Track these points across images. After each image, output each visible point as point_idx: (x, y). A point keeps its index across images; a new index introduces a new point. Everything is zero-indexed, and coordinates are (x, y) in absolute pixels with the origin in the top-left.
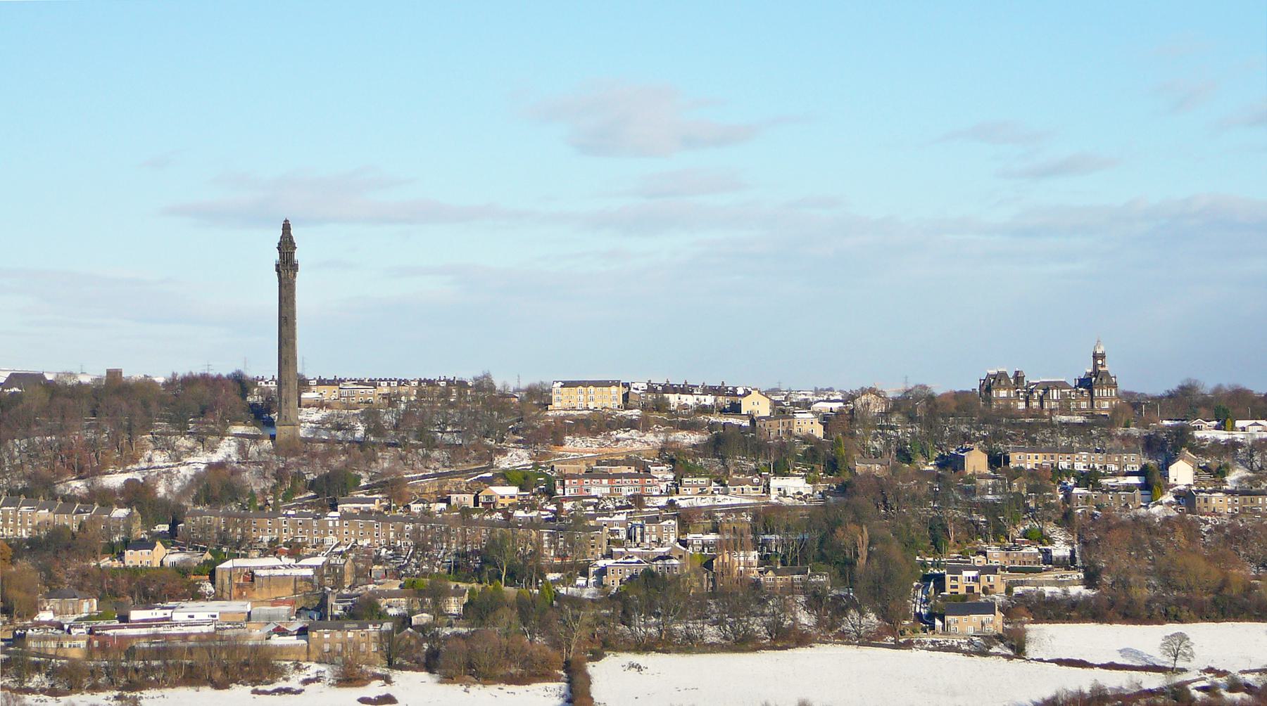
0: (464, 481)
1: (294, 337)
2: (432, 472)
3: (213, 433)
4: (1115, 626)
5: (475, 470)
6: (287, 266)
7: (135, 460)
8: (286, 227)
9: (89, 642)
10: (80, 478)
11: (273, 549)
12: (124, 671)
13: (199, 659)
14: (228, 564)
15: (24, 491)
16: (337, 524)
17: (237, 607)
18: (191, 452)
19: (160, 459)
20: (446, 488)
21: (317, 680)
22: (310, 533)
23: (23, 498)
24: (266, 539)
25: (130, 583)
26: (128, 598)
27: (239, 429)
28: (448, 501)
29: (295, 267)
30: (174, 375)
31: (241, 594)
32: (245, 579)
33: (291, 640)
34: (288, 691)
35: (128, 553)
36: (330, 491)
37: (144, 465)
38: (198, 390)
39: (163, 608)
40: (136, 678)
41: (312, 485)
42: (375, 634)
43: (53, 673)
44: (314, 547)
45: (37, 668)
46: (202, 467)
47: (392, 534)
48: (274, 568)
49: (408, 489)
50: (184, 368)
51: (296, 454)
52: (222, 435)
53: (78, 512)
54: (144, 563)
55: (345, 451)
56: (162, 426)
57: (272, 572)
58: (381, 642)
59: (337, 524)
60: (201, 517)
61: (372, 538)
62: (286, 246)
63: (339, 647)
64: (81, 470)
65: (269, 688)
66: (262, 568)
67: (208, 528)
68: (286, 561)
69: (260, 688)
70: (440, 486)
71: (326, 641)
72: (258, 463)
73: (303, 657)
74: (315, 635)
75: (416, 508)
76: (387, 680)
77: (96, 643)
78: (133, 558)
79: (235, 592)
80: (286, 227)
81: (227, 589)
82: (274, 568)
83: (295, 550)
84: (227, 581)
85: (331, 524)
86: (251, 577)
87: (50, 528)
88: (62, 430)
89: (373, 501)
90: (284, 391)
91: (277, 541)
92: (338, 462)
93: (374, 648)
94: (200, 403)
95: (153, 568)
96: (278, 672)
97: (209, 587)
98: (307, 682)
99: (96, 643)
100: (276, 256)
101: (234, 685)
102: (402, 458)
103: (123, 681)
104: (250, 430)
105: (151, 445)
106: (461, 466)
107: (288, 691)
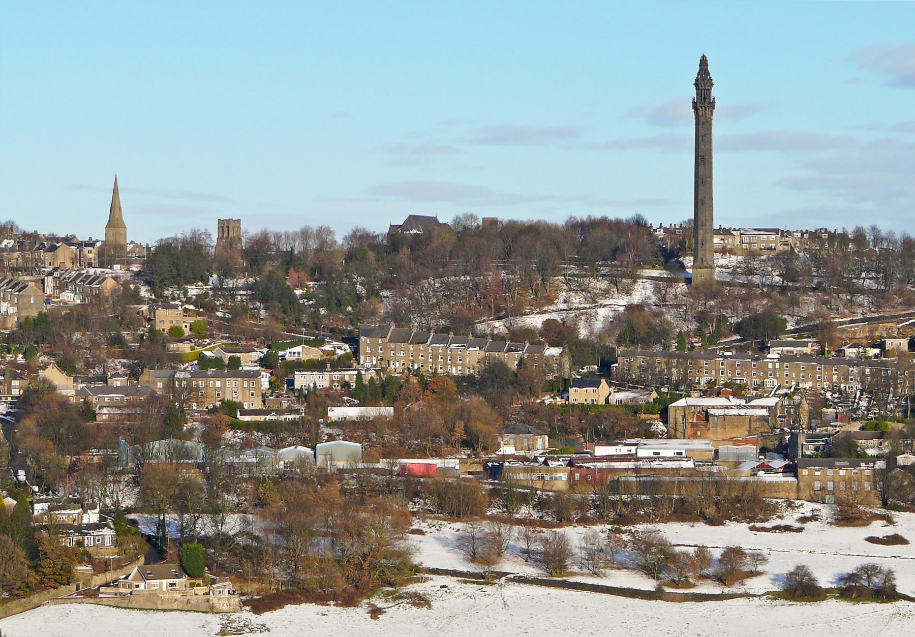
0: (895, 326)
1: (710, 176)
2: (859, 317)
3: (624, 276)
4: (303, 605)
5: (904, 315)
6: (703, 103)
7: (550, 302)
8: (704, 62)
9: (571, 474)
10: (499, 318)
11: (711, 390)
12: (614, 504)
13: (692, 495)
14: (681, 403)
15: (445, 330)
16: (777, 366)
17: (701, 445)
18: (606, 293)
19: (577, 300)
20: (877, 333)
21: (814, 518)
22: (749, 375)
23: (451, 335)
24: (703, 381)
25: (580, 420)
26: (579, 435)
27: (655, 273)
28: (882, 346)
29: (712, 105)
30: (589, 216)
31: (695, 434)
32: (698, 418)
33: (778, 478)
34: (787, 528)
35: (572, 390)
36: (757, 334)
37: (564, 306)
38: (599, 232)
39: (626, 445)
40: (625, 511)
41: (738, 328)
42: (868, 472)
43: (542, 505)
44: (755, 389)
45: (524, 499)
46: (622, 309)
47: (835, 377)
48: (727, 407)
49: (838, 334)
50: (582, 213)
51: (713, 297)
52: (635, 278)
53: (510, 350)
54: (589, 402)
55: (767, 295)
56: (573, 269)
57: (727, 412)
58: (875, 482)
59: (777, 366)
60: (629, 361)
61: (815, 381)
62: (703, 82)
63: (842, 486)
64: (498, 310)
65: (767, 525)
66: (713, 407)
67: (644, 366)
68: (735, 401)
69: (758, 525)
70: (871, 331)
71: (817, 479)
72: (678, 306)
73: (792, 495)
74: (805, 472)
75: (851, 352)
76: (890, 521)
77: (577, 476)
78: (577, 396)
79: (689, 431)
80: (704, 62)
81: (680, 428)
82: (727, 407)
83: (738, 391)
84: (680, 420)
85: (770, 366)
86: (706, 416)
87: (492, 362)
88: (477, 269)
89: (805, 345)
90: (701, 232)
91: (715, 383)
92: (760, 306)
93: (867, 486)
94: (608, 246)
95: (597, 406)
96: (770, 510)
97: (660, 427)
98: (804, 520)
99: (577, 476)
100: (693, 92)
101: (728, 522)
102: (826, 303)
103: (612, 514)
104: (664, 274)
105: (565, 287)
106: (887, 312)
107: (787, 528)
